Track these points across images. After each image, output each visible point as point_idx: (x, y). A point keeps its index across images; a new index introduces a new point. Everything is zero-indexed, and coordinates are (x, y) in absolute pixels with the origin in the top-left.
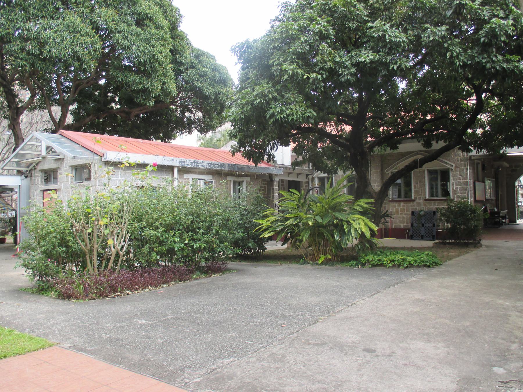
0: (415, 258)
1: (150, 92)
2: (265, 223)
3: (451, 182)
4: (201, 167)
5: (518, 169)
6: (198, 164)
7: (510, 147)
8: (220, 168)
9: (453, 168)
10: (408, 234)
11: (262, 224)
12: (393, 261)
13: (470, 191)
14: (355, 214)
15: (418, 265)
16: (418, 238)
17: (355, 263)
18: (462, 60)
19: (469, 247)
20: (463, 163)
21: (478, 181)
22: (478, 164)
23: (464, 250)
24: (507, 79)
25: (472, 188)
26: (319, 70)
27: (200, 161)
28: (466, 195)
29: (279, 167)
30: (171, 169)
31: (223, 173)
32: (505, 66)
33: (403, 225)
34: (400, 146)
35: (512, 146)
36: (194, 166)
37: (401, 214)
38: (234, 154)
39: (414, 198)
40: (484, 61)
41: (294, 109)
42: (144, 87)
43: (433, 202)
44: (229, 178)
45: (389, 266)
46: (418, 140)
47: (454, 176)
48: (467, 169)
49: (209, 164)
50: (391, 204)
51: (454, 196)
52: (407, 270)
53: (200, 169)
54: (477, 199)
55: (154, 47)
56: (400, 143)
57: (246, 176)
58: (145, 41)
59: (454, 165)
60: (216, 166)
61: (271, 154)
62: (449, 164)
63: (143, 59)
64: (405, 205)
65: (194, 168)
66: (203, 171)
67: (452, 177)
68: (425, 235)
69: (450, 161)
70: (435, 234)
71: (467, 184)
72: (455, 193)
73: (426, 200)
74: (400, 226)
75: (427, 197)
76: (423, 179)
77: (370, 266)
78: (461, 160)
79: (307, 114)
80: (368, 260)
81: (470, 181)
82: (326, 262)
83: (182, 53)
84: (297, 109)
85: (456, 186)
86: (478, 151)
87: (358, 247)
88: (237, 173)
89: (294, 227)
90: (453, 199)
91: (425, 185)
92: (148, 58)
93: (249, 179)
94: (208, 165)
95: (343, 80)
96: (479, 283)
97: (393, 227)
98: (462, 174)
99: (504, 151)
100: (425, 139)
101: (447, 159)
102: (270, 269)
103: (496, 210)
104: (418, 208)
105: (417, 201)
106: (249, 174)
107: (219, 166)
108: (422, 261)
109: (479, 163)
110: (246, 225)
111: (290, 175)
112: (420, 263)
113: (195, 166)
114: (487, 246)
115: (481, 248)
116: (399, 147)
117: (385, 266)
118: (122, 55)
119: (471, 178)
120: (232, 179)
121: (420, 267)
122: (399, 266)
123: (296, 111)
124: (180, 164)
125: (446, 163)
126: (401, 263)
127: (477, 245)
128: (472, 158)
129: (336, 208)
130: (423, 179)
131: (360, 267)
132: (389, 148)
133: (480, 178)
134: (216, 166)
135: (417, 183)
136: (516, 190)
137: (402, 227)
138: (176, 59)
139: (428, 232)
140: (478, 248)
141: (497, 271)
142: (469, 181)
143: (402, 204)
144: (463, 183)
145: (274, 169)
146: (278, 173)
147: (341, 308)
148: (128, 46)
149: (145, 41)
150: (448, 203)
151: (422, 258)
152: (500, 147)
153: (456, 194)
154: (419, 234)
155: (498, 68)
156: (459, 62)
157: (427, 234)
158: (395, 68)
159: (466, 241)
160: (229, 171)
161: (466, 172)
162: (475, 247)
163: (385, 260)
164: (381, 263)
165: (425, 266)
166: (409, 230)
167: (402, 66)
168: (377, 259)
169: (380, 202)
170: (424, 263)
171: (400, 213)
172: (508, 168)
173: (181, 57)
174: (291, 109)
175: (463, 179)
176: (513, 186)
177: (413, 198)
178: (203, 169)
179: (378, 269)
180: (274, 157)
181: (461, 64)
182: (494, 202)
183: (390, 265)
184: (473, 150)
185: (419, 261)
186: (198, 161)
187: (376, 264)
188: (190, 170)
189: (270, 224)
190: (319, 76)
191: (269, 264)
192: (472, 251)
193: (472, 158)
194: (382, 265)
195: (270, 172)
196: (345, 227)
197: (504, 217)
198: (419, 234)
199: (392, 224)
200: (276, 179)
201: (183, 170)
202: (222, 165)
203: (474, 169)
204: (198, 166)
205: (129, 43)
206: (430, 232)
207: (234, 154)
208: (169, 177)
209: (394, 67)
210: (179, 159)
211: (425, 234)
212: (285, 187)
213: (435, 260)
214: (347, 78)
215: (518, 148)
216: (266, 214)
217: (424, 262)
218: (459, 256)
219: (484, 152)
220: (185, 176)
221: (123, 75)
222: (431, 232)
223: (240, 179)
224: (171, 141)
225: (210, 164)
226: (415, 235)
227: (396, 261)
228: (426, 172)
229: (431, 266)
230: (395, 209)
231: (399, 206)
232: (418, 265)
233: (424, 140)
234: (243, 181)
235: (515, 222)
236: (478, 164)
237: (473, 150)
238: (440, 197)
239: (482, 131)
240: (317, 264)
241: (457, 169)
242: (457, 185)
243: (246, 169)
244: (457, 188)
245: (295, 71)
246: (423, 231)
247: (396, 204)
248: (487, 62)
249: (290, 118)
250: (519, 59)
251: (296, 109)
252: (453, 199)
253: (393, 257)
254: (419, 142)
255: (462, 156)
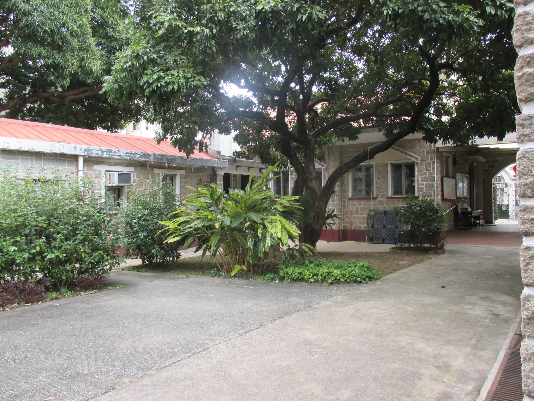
0: (344, 272)
1: (63, 69)
2: (171, 225)
3: (416, 177)
4: (116, 157)
5: (496, 164)
6: (111, 154)
7: (479, 136)
8: (143, 159)
9: (419, 161)
10: (368, 235)
11: (168, 226)
12: (317, 275)
13: (437, 188)
14: (275, 215)
15: (346, 280)
16: (378, 241)
17: (272, 276)
18: (392, 7)
19: (429, 254)
20: (429, 155)
21: (447, 176)
22: (447, 157)
23: (422, 257)
24: (453, 37)
25: (440, 185)
26: (208, 23)
27: (114, 149)
28: (432, 192)
29: (223, 159)
30: (74, 158)
31: (148, 165)
32: (450, 19)
33: (364, 226)
34: (360, 136)
35: (481, 136)
36: (105, 155)
37: (361, 214)
38: (159, 143)
39: (376, 195)
40: (420, 9)
41: (176, 75)
42: (54, 62)
43: (396, 200)
44: (156, 171)
45: (311, 282)
46: (379, 129)
47: (419, 170)
48: (434, 163)
49: (127, 153)
50: (351, 202)
51: (420, 194)
52: (331, 287)
53: (116, 159)
54: (445, 197)
55: (63, 14)
56: (359, 133)
57: (181, 168)
58: (53, 6)
59: (420, 158)
60: (137, 156)
61: (203, 143)
62: (414, 157)
63: (50, 28)
64: (366, 203)
65: (108, 158)
66: (120, 161)
67: (417, 171)
68: (387, 238)
69: (415, 153)
70: (397, 236)
71: (433, 179)
72: (420, 190)
73: (388, 198)
74: (361, 227)
75: (390, 194)
76: (386, 174)
77: (289, 281)
78: (428, 153)
79: (195, 83)
80: (287, 273)
81: (437, 177)
82: (240, 275)
83: (114, 27)
84: (180, 75)
85: (422, 182)
86: (444, 141)
87: (285, 256)
88: (167, 165)
89: (207, 229)
90: (418, 198)
91: (387, 181)
92: (56, 26)
93: (183, 172)
94: (125, 154)
95: (239, 36)
96: (410, 309)
97: (353, 228)
98: (428, 168)
99: (472, 142)
100: (387, 128)
101: (412, 152)
102: (179, 282)
103: (469, 209)
104: (380, 207)
105: (379, 199)
106: (184, 166)
107: (141, 156)
108: (351, 275)
109: (449, 157)
110: (150, 227)
111: (239, 168)
112: (348, 278)
113: (108, 156)
114: (451, 252)
115: (442, 255)
116: (359, 138)
117: (307, 281)
118: (22, 22)
119: (439, 173)
120: (161, 173)
121: (348, 283)
122: (323, 281)
123: (178, 78)
124: (86, 153)
125: (411, 156)
126: (325, 278)
127: (439, 250)
128: (440, 150)
129: (256, 207)
130: (386, 174)
131: (277, 281)
132: (348, 138)
133: (451, 173)
134: (137, 156)
135: (379, 179)
136: (494, 188)
137: (362, 229)
138: (107, 34)
139: (390, 235)
140: (439, 254)
141: (443, 289)
142: (436, 176)
143: (363, 202)
144: (430, 179)
145: (216, 162)
146: (221, 166)
147: (181, 356)
148: (29, 11)
149: (53, 6)
150: (407, 201)
151: (352, 271)
152: (469, 136)
153: (421, 191)
154: (380, 236)
155: (441, 21)
156: (387, 10)
157: (388, 236)
158: (304, 19)
159: (428, 245)
160: (155, 162)
161: (433, 166)
162: (435, 253)
163: (307, 273)
164: (302, 276)
165: (355, 281)
166: (369, 231)
167: (313, 17)
168: (297, 271)
169: (325, 200)
170: (354, 278)
171: (360, 212)
172: (485, 163)
173: (113, 31)
174: (173, 75)
175: (429, 174)
176: (490, 183)
177: (375, 196)
178: (119, 159)
179: (298, 284)
180: (207, 146)
181: (390, 12)
182: (468, 201)
183: (312, 280)
184: (439, 141)
185: (348, 275)
186: (112, 149)
187: (296, 279)
188: (108, 161)
189: (177, 226)
190: (207, 31)
191: (178, 276)
192: (430, 258)
193: (440, 150)
194: (302, 280)
195: (211, 165)
196: (259, 231)
197: (478, 218)
198: (380, 236)
199: (352, 225)
200: (221, 173)
201: (90, 161)
202: (145, 155)
203: (442, 163)
204: (112, 155)
205: (30, 8)
206: (392, 235)
207: (159, 143)
208: (73, 168)
209: (302, 17)
210: (85, 147)
211: (387, 236)
212: (238, 182)
213: (370, 274)
214: (244, 33)
215: (489, 138)
216: (178, 213)
217: (354, 276)
218: (410, 265)
219: (450, 144)
220: (96, 167)
221: (26, 46)
222: (393, 235)
223: (172, 172)
224: (118, 131)
225: (129, 153)
226: (375, 238)
227: (320, 275)
228: (389, 167)
229: (363, 281)
230: (354, 207)
231: (360, 204)
232: (346, 280)
233: (386, 130)
234: (176, 175)
235: (491, 222)
236: (447, 157)
237: (439, 141)
238: (404, 195)
239: (449, 118)
240: (229, 276)
241: (423, 162)
242: (422, 180)
243: (179, 160)
244: (422, 184)
245: (174, 23)
246: (384, 233)
247: (356, 203)
248: (425, 11)
249: (171, 87)
250: (470, 9)
251: (178, 76)
252: (418, 198)
253: (315, 271)
254: (380, 131)
255: (428, 148)
